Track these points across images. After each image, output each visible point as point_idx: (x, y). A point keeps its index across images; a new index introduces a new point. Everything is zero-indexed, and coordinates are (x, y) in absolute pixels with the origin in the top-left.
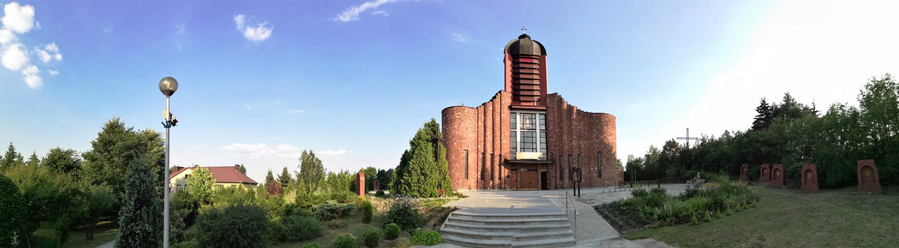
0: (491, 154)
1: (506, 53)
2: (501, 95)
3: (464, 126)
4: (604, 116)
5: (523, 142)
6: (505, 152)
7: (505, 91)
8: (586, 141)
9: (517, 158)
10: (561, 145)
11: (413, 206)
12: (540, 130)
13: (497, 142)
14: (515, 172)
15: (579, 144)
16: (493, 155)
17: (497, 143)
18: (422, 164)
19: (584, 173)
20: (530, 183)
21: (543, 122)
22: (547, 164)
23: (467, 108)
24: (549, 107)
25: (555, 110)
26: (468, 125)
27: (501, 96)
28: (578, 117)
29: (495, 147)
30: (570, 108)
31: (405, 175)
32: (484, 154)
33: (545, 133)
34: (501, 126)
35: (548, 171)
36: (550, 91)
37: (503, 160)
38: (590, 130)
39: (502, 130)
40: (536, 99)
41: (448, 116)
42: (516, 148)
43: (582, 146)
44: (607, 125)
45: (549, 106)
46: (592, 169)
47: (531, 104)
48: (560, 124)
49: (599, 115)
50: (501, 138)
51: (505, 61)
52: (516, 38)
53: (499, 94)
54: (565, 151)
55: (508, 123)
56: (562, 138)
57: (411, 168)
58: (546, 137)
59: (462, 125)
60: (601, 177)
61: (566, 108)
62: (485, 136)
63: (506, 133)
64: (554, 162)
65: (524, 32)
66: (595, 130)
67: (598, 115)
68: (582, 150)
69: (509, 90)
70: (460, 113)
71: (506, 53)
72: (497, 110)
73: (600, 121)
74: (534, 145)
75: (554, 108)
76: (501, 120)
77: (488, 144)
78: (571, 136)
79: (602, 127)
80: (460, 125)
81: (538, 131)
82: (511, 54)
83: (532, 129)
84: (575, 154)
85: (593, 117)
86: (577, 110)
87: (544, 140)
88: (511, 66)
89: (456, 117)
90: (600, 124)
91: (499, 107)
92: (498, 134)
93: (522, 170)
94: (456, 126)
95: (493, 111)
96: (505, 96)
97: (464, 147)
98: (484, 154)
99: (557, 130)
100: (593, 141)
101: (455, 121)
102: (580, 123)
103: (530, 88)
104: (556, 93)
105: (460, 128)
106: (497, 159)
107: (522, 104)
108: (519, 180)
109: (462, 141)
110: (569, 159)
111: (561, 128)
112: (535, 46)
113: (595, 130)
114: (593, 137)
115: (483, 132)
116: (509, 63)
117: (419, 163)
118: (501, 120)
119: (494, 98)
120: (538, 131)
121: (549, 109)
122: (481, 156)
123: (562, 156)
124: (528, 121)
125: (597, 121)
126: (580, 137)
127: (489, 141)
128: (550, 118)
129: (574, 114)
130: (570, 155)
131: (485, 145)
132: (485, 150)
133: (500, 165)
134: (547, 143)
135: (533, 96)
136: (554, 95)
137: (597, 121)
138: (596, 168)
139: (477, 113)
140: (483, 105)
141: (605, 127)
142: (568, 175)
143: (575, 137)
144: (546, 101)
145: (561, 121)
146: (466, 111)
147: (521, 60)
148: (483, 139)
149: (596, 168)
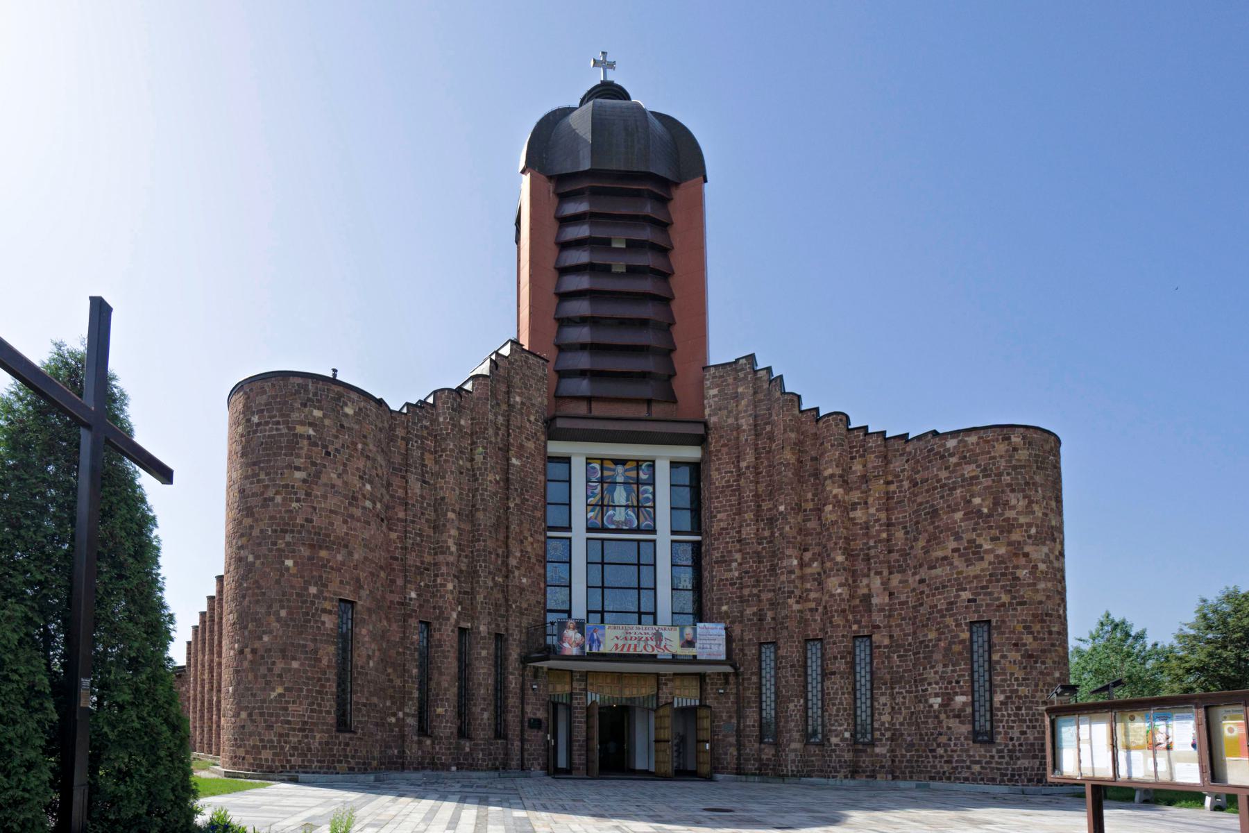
8: (1053, 523)
11: (220, 812)
12: (673, 533)
33: (689, 548)
35: (703, 705)
43: (875, 601)
46: (936, 702)
48: (766, 506)
66: (959, 515)
67: (973, 439)
70: (317, 413)
80: (318, 475)
83: (638, 530)
87: (686, 579)
89: (300, 429)
97: (334, 587)
113: (959, 515)
124: (620, 496)
138: (960, 699)
144: (703, 397)
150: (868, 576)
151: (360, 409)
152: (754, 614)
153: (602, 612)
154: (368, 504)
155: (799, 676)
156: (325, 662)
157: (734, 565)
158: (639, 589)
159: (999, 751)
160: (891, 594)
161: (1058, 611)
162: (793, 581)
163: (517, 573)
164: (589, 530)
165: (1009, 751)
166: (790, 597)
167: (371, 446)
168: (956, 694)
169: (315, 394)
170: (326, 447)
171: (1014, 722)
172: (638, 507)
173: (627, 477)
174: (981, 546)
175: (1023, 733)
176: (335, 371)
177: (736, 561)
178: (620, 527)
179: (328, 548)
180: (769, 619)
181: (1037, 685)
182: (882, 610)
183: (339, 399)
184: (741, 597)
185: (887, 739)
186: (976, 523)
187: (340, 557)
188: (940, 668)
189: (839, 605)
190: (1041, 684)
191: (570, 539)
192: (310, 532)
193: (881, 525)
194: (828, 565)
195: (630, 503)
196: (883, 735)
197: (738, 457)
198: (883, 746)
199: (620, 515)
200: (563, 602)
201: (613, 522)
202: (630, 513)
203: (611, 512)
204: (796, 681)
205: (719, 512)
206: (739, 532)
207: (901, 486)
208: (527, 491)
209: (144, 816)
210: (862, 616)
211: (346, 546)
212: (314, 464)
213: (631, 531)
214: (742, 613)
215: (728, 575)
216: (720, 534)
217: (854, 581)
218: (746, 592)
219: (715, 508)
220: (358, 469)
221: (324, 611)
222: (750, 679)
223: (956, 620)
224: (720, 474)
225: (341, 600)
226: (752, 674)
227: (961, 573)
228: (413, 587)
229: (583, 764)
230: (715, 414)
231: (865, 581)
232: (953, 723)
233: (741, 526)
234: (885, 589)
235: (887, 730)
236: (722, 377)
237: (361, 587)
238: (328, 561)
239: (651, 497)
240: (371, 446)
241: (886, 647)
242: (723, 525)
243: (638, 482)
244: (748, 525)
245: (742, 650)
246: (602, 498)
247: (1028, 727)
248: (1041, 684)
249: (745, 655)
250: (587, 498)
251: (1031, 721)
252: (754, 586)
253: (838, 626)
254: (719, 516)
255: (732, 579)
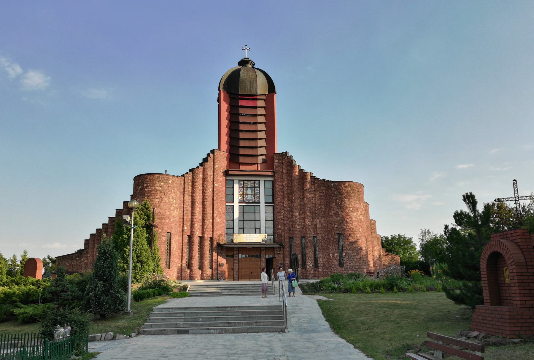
0: (200, 237)
1: (222, 91)
2: (214, 156)
3: (167, 201)
4: (344, 185)
5: (242, 220)
6: (219, 234)
7: (219, 148)
9: (235, 241)
10: (291, 223)
12: (265, 203)
13: (209, 221)
14: (232, 259)
15: (315, 223)
16: (202, 239)
17: (208, 223)
18: (139, 251)
19: (321, 260)
20: (251, 273)
21: (270, 192)
22: (274, 247)
23: (172, 177)
24: (277, 172)
25: (284, 176)
26: (172, 200)
27: (214, 158)
28: (313, 187)
29: (205, 227)
30: (303, 174)
31: (120, 262)
32: (191, 237)
33: (272, 207)
34: (213, 199)
35: (274, 257)
36: (279, 149)
37: (215, 244)
38: (328, 205)
39: (215, 205)
40: (260, 159)
41: (145, 185)
42: (233, 228)
43: (318, 226)
44: (350, 197)
45: (277, 169)
46: (331, 255)
47: (254, 167)
49: (339, 184)
50: (213, 216)
51: (219, 100)
52: (236, 66)
53: (212, 155)
54: (297, 233)
55: (223, 195)
56: (292, 215)
57: (127, 255)
58: (273, 213)
59: (165, 200)
60: (343, 266)
61: (297, 174)
62: (193, 214)
63: (220, 209)
64: (282, 246)
65: (246, 55)
66: (334, 204)
67: (337, 184)
68: (318, 231)
69: (225, 147)
70: (162, 184)
71: (222, 91)
72: (208, 178)
73: (340, 193)
74: (257, 215)
75: (283, 173)
76: (213, 191)
77: (196, 225)
78: (304, 212)
79: (342, 201)
80: (162, 200)
81: (262, 204)
82: (228, 92)
83: (255, 202)
84: (310, 234)
85: (331, 187)
86: (311, 177)
87: (270, 216)
88: (227, 111)
90: (340, 196)
91: (212, 172)
92: (209, 210)
93: (241, 256)
94: (157, 200)
95: (204, 179)
96: (219, 157)
97: (166, 229)
98: (191, 237)
99: (286, 204)
100: (331, 219)
101: (155, 194)
102: (315, 194)
103: (252, 144)
104: (286, 152)
105: (162, 204)
106: (207, 243)
107: (242, 168)
108: (236, 268)
109: (163, 221)
110: (302, 242)
111: (292, 201)
112: (261, 80)
113: (334, 204)
114: (331, 214)
115: (190, 209)
116: (225, 106)
117: (136, 250)
118: (213, 191)
119: (205, 160)
120: (262, 204)
121: (276, 175)
122: (186, 240)
123: (293, 238)
124: (249, 192)
125: (336, 192)
126: (315, 214)
127: (198, 220)
128: (278, 187)
129: (308, 184)
130: (302, 237)
131: (192, 226)
132: (192, 232)
133: (211, 251)
134: (274, 220)
135: (257, 156)
136: (284, 155)
137: (336, 192)
138: (336, 254)
139: (183, 182)
140: (190, 170)
141: (347, 201)
142: (301, 263)
143: (308, 214)
145: (292, 192)
146: (170, 182)
147: (242, 103)
148: (190, 217)
149: (336, 254)
150: (316, 218)
151: (173, 181)
152: (288, 229)
153: (244, 228)
154: (175, 205)
155: (299, 248)
156: (163, 250)
157: (282, 214)
158: (255, 220)
159: (345, 269)
160: (322, 224)
161: (359, 230)
162: (297, 220)
163: (216, 218)
164: (239, 203)
165: (347, 269)
166: (296, 224)
167: (176, 190)
168: (335, 253)
169: (162, 179)
170: (164, 192)
171: (348, 261)
172: (255, 195)
173: (251, 186)
174: (339, 213)
175: (350, 264)
176: (166, 171)
177: (283, 212)
178: (249, 201)
179: (164, 219)
180: (292, 230)
181: (353, 251)
182: (319, 229)
183: (167, 179)
184: (284, 223)
185: (322, 266)
186: (338, 207)
187: (167, 221)
188: (332, 246)
189: (308, 227)
190: (354, 250)
191: (234, 205)
192: (159, 215)
193: (319, 205)
194: (305, 215)
195: (252, 194)
196: (320, 265)
197: (283, 181)
198: (321, 268)
199: (249, 198)
200: (231, 225)
201: (247, 200)
202: (252, 197)
203: (246, 197)
204: (298, 249)
205: (278, 197)
206: (283, 204)
207: (323, 194)
208: (220, 193)
209: (56, 309)
210: (315, 230)
211: (169, 218)
212: (161, 197)
213: (252, 203)
214: (284, 228)
215: (280, 217)
216: (278, 204)
217: (313, 220)
218: (285, 222)
219: (277, 196)
220: (172, 197)
221: (163, 236)
222: (287, 249)
223: (334, 233)
224: (278, 186)
225: (167, 233)
226: (287, 247)
227: (335, 220)
228: (186, 226)
229: (237, 278)
230: (277, 168)
231: (315, 220)
232: (335, 261)
233: (284, 202)
234: (320, 223)
235: (322, 263)
236: (278, 157)
237: (172, 228)
238: (164, 222)
239: (259, 192)
240: (176, 190)
241: (321, 239)
242: (279, 201)
243: (255, 187)
244: (286, 202)
245: (284, 240)
246: (243, 193)
247: (351, 262)
248: (354, 250)
249: (285, 241)
250: (239, 192)
251: (352, 260)
252: (287, 220)
253: (308, 233)
254: (278, 199)
255: (282, 218)
